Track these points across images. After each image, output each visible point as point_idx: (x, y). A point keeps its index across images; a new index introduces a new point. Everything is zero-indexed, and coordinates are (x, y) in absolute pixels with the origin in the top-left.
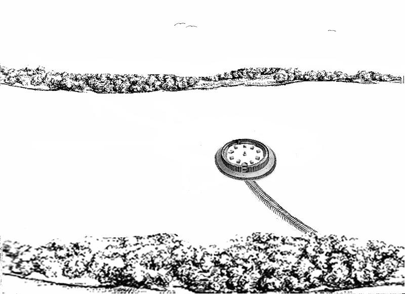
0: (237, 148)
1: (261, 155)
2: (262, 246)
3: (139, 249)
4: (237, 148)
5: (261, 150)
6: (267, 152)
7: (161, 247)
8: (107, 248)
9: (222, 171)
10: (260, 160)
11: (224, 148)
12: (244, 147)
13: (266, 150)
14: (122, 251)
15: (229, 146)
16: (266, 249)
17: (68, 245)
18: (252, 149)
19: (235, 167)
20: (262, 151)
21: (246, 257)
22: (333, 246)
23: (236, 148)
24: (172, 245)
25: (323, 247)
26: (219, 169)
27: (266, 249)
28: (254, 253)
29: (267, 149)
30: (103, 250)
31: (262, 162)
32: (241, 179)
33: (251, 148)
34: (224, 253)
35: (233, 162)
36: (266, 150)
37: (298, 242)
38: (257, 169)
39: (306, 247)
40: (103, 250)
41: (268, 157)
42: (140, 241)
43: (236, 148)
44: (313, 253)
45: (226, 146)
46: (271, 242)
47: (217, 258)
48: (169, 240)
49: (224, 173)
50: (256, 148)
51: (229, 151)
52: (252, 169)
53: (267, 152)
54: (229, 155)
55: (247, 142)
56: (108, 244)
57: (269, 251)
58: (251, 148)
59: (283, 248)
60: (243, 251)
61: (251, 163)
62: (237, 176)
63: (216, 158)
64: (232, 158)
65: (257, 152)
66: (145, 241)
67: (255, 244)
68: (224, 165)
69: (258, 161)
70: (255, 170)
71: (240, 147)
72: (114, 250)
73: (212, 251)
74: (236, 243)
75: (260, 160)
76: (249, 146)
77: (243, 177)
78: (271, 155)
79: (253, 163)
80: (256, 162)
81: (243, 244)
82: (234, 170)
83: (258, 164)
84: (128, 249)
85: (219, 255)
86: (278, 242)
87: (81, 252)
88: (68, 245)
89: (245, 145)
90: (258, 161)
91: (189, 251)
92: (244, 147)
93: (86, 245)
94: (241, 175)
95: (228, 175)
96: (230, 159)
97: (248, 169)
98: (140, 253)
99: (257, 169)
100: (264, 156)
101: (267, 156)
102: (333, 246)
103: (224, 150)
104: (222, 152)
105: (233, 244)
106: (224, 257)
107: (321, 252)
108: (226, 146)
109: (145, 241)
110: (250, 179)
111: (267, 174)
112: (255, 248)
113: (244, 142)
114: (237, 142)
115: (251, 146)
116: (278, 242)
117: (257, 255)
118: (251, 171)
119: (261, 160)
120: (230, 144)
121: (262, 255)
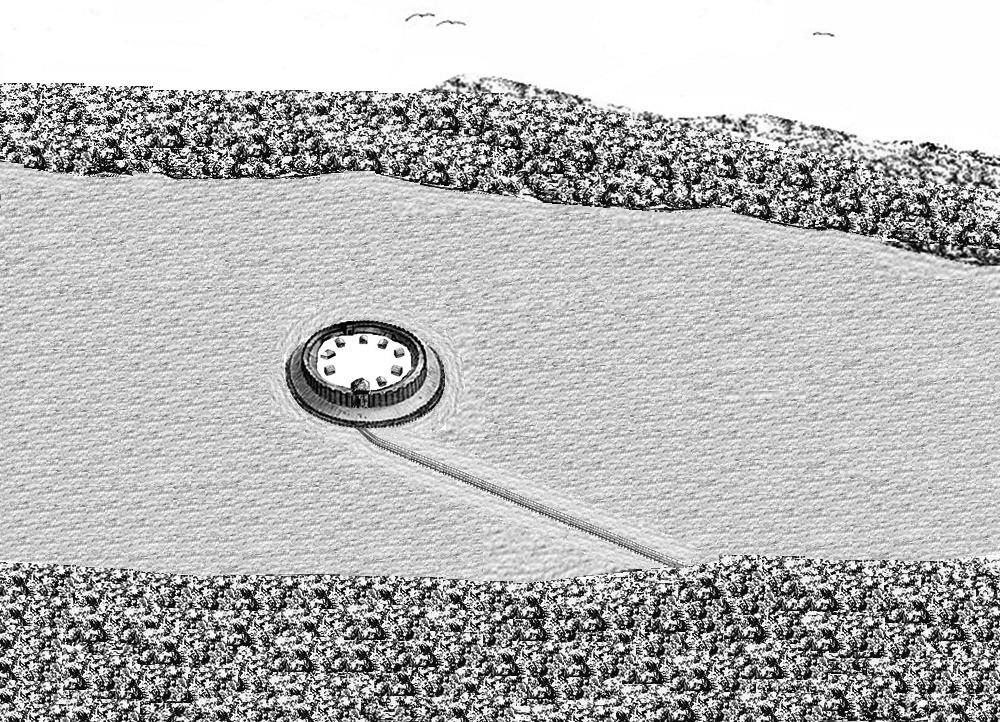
0: (343, 344)
1: (405, 362)
2: (917, 162)
3: (801, 139)
4: (343, 344)
5: (405, 349)
6: (421, 356)
7: (823, 142)
8: (772, 131)
9: (304, 405)
10: (403, 375)
11: (309, 345)
12: (362, 341)
13: (419, 349)
14: (786, 138)
15: (323, 340)
16: (920, 166)
17: (736, 120)
18: (383, 346)
19: (338, 395)
20: (408, 353)
21: (899, 169)
22: (983, 178)
23: (340, 345)
24: (833, 142)
25: (973, 176)
26: (297, 397)
27: (920, 166)
28: (907, 167)
29: (422, 347)
30: (768, 132)
31: (407, 381)
32: (352, 424)
33: (380, 346)
34: (880, 161)
35: (334, 381)
36: (419, 349)
37: (951, 166)
38: (395, 399)
39: (957, 172)
40: (768, 132)
41: (425, 368)
42: (805, 132)
43: (340, 345)
44: (962, 180)
45: (315, 338)
46: (926, 160)
47: (873, 164)
48: (832, 137)
49: (310, 409)
50: (393, 346)
51: (322, 351)
52: (383, 399)
53: (421, 356)
54: (322, 364)
55: (371, 329)
56: (774, 128)
57: (922, 168)
58: (380, 346)
59: (936, 169)
60: (898, 163)
61: (380, 384)
62: (342, 416)
63: (288, 369)
64: (330, 370)
65: (396, 354)
66: (809, 133)
67: (910, 158)
68: (311, 390)
69: (399, 379)
70: (389, 401)
71: (352, 341)
72: (778, 135)
73: (869, 156)
74: (893, 154)
75: (403, 375)
76: (374, 340)
77: (359, 420)
78: (432, 362)
79: (385, 383)
80: (392, 380)
81: (899, 156)
82: (335, 403)
83: (397, 387)
84: (792, 136)
85: (875, 162)
86: (933, 162)
87: (748, 129)
88: (736, 120)
89: (365, 336)
90: (399, 379)
91: (847, 152)
92: (362, 341)
93: (754, 124)
94: (353, 414)
95: (322, 416)
96: (326, 372)
97: (378, 400)
98: (802, 143)
99: (395, 399)
100: (414, 364)
101: (420, 366)
102: (983, 178)
103: (311, 349)
104: (306, 355)
105: (890, 153)
106: (879, 165)
107: (970, 180)
108: (315, 338)
109: (809, 133)
110: (376, 424)
111: (421, 412)
112: (909, 163)
113: (362, 330)
114: (344, 328)
115: (380, 339)
116: (933, 162)
117: (910, 170)
118: (380, 405)
119: (407, 376)
120: (325, 335)
121: (914, 171)
